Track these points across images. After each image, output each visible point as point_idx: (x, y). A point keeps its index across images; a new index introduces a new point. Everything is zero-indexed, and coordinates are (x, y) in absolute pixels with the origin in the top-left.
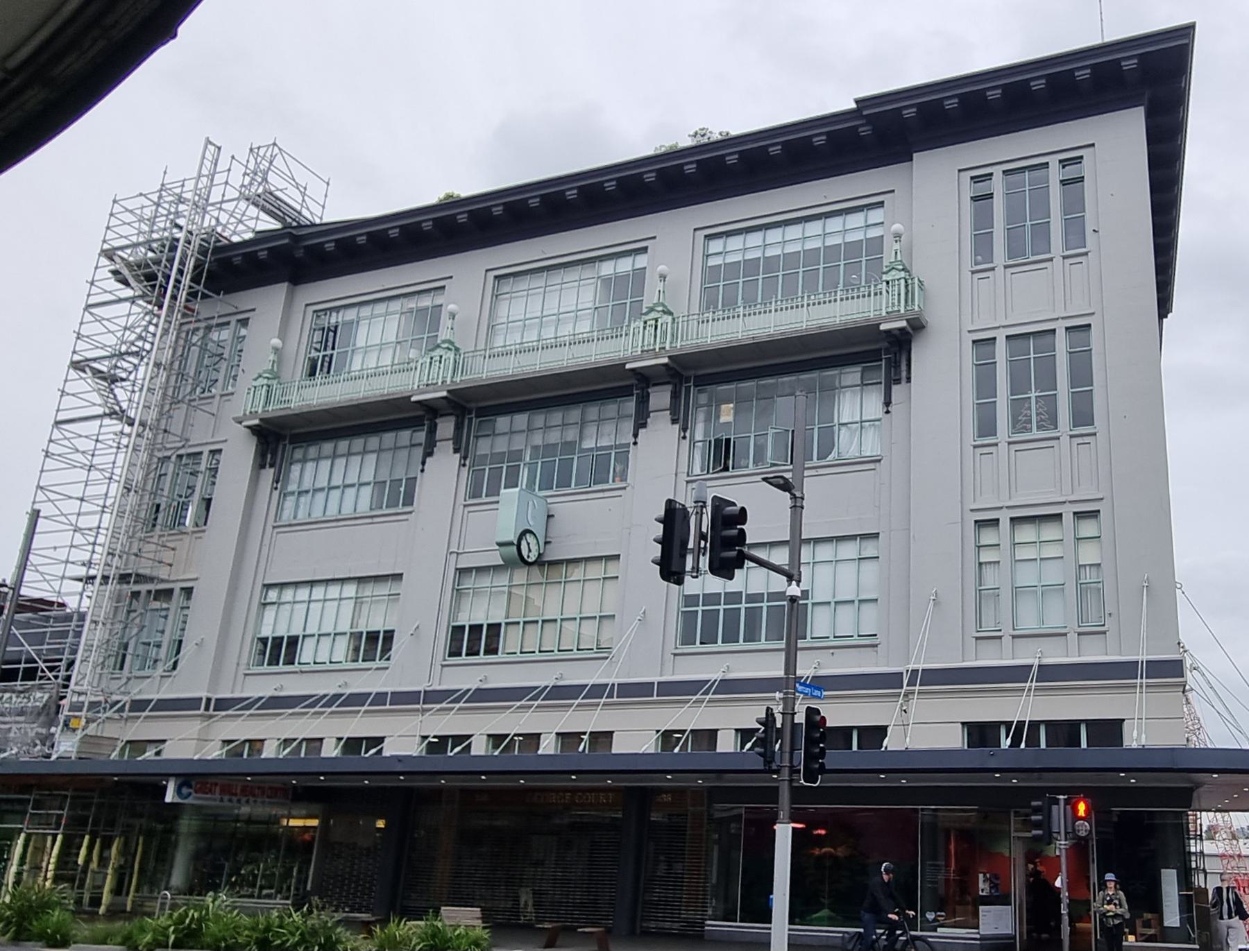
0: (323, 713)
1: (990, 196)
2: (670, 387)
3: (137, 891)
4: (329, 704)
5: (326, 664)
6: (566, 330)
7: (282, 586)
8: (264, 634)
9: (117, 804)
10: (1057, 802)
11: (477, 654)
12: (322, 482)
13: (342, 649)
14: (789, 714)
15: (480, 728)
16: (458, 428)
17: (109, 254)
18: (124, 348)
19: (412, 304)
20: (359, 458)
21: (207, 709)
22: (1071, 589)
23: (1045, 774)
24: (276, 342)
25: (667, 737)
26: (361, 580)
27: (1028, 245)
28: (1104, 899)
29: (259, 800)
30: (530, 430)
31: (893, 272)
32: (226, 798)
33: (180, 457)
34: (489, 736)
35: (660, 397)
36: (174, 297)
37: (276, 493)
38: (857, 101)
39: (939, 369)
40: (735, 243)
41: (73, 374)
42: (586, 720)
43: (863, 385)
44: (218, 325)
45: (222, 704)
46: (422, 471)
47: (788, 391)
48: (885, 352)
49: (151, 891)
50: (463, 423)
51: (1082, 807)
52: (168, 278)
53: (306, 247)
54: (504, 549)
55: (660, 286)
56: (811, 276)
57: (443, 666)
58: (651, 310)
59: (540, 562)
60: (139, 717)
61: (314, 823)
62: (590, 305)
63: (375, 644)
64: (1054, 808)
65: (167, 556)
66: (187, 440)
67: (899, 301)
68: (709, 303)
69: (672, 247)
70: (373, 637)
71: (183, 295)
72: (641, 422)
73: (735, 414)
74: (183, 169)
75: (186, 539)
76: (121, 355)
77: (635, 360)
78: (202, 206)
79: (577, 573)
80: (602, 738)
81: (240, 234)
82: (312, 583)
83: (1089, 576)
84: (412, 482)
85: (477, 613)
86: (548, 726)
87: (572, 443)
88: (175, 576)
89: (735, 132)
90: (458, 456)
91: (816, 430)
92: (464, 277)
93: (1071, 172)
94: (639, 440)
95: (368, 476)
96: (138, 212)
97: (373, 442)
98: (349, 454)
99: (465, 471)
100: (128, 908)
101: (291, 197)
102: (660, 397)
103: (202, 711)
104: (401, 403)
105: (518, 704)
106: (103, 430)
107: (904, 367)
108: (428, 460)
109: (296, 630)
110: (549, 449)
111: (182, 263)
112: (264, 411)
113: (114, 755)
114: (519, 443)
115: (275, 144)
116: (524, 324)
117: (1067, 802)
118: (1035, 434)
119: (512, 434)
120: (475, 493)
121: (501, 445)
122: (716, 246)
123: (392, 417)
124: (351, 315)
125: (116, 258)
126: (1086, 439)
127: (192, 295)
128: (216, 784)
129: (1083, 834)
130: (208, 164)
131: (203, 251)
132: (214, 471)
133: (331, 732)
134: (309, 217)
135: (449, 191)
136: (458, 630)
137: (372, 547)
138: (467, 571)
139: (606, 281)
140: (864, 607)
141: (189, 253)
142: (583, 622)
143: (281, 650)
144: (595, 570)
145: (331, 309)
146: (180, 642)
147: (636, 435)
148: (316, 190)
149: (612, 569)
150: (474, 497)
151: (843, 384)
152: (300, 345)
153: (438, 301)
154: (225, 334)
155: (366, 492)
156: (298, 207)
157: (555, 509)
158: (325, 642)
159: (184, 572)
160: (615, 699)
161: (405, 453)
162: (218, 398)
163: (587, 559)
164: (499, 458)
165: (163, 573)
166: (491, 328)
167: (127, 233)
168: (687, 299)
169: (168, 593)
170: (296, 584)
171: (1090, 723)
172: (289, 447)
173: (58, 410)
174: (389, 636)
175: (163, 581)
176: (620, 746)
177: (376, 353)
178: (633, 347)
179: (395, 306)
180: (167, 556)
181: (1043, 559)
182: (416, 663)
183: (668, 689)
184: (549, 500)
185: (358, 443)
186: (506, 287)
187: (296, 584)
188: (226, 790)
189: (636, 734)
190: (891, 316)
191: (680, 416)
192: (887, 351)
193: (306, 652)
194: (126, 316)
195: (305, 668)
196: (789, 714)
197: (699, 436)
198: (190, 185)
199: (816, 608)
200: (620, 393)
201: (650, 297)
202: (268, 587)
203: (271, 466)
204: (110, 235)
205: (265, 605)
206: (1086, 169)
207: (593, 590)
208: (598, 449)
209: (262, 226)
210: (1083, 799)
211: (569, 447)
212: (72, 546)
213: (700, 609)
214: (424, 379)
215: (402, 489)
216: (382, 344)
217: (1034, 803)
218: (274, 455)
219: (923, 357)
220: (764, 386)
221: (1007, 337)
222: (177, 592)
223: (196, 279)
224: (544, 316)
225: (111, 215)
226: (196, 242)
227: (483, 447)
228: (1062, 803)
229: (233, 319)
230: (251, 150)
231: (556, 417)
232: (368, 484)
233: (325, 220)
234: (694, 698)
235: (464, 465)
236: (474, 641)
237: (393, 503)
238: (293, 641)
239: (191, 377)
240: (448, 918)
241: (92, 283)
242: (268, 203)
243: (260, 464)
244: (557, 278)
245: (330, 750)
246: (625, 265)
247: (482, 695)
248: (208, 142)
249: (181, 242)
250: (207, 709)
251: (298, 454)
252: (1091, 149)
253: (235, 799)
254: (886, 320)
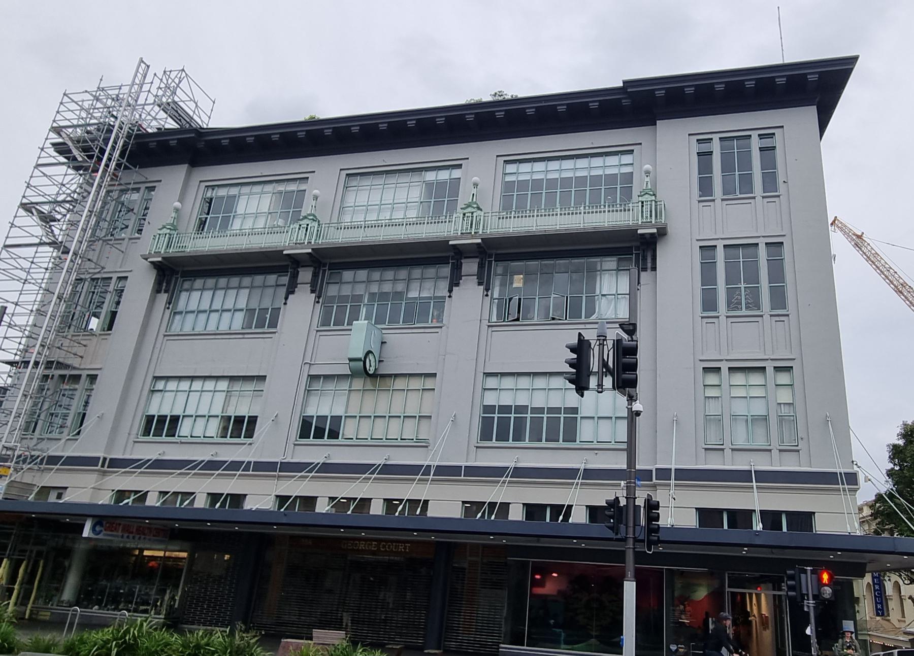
0: (307, 477)
1: (710, 153)
2: (312, 269)
3: (33, 603)
4: (247, 469)
5: (200, 436)
6: (399, 215)
7: (168, 378)
8: (151, 413)
9: (36, 536)
10: (805, 572)
11: (323, 437)
12: (205, 305)
13: (214, 427)
14: (631, 498)
15: (325, 493)
16: (315, 275)
17: (58, 130)
18: (60, 198)
19: (281, 188)
20: (223, 292)
21: (103, 466)
22: (773, 420)
23: (542, 539)
24: (177, 204)
25: (282, 499)
26: (232, 379)
27: (740, 187)
28: (843, 645)
29: (148, 537)
30: (369, 281)
31: (647, 196)
32: (126, 535)
33: (93, 280)
34: (208, 494)
35: (470, 266)
36: (107, 166)
37: (168, 312)
38: (624, 82)
39: (677, 264)
40: (525, 167)
41: (22, 212)
42: (229, 486)
43: (618, 270)
44: (133, 189)
45: (115, 463)
46: (285, 304)
47: (563, 270)
48: (637, 249)
49: (46, 603)
50: (319, 273)
51: (825, 577)
52: (102, 152)
53: (206, 141)
54: (352, 364)
55: (314, 203)
56: (581, 194)
57: (135, 442)
58: (305, 217)
59: (374, 376)
60: (52, 469)
61: (185, 555)
62: (417, 200)
63: (241, 427)
64: (803, 576)
65: (80, 351)
66: (103, 268)
67: (651, 216)
68: (506, 206)
69: (481, 169)
70: (239, 420)
71: (113, 165)
72: (291, 290)
73: (524, 283)
74: (121, 75)
75: (95, 339)
76: (59, 203)
77: (456, 238)
78: (132, 107)
79: (400, 384)
80: (237, 499)
81: (151, 127)
82: (193, 378)
83: (785, 411)
84: (276, 311)
85: (323, 406)
86: (377, 493)
87: (401, 293)
88: (85, 366)
89: (520, 96)
90: (314, 295)
91: (584, 298)
92: (324, 175)
93: (767, 143)
94: (288, 302)
95: (242, 304)
96: (80, 103)
97: (247, 281)
98: (227, 288)
99: (318, 306)
100: (27, 617)
101: (189, 107)
102: (470, 266)
103: (99, 467)
104: (276, 255)
105: (300, 474)
106: (37, 255)
107: (649, 260)
108: (290, 296)
109: (178, 411)
110: (383, 296)
111: (115, 142)
112: (165, 252)
113: (31, 498)
114: (360, 290)
115: (183, 70)
116: (367, 208)
117: (812, 572)
118: (744, 312)
119: (354, 283)
120: (325, 322)
121: (346, 290)
122: (511, 168)
123: (240, 266)
124: (234, 191)
125: (62, 133)
126: (782, 318)
127: (119, 165)
128: (120, 524)
129: (827, 596)
130: (139, 76)
131: (129, 136)
132: (120, 292)
133: (202, 489)
134: (200, 123)
135: (313, 114)
136: (150, 419)
137: (245, 355)
138: (317, 377)
139: (429, 185)
140: (378, 420)
141: (121, 135)
142: (362, 420)
143: (163, 426)
144: (416, 384)
145: (218, 186)
146: (84, 414)
147: (450, 291)
148: (205, 104)
149: (429, 383)
150: (323, 325)
151: (604, 268)
152: (193, 208)
153: (303, 187)
154: (135, 196)
155: (239, 316)
156: (191, 113)
157: (387, 338)
158: (201, 422)
159: (91, 363)
160: (462, 477)
161: (271, 290)
162: (127, 240)
163: (411, 375)
164: (343, 299)
165: (75, 362)
166: (342, 208)
167: (71, 117)
168: (492, 201)
169: (76, 378)
170: (180, 378)
171: (789, 514)
172: (180, 280)
173: (7, 237)
174: (253, 420)
175: (75, 368)
176: (433, 512)
177: (252, 220)
178: (451, 229)
179: (269, 188)
180: (80, 351)
181: (745, 397)
182: (273, 442)
183: (472, 471)
184: (384, 331)
185: (235, 281)
186: (354, 182)
187: (180, 378)
188: (127, 529)
189: (445, 503)
190: (645, 225)
191: (484, 281)
192: (637, 248)
193: (185, 428)
194: (63, 179)
195: (183, 440)
196: (631, 498)
197: (496, 295)
198: (125, 90)
199: (348, 419)
200: (440, 261)
201: (463, 198)
202: (157, 378)
203: (166, 291)
204: (59, 117)
205: (153, 391)
206: (778, 141)
207: (414, 398)
208: (420, 298)
209: (167, 126)
210: (826, 570)
211: (398, 295)
212: (5, 338)
213: (513, 416)
214: (291, 239)
215: (268, 316)
216: (255, 214)
217: (788, 572)
218: (168, 284)
219: (665, 254)
220: (545, 265)
221: (724, 246)
222: (84, 378)
223: (122, 155)
224: (383, 205)
225: (61, 103)
226: (126, 129)
227: (332, 290)
228: (809, 573)
229: (143, 186)
230: (165, 72)
231: (389, 274)
232: (242, 310)
233: (210, 126)
234: (364, 476)
235: (318, 302)
236: (313, 429)
237: (261, 325)
238: (175, 420)
239: (115, 223)
240: (318, 637)
241: (42, 149)
242: (173, 110)
243: (157, 289)
244: (392, 179)
245: (201, 502)
246: (444, 175)
247: (327, 468)
248: (142, 61)
249: (116, 127)
250: (103, 466)
251: (187, 285)
252: (781, 130)
253: (131, 536)
254: (642, 227)
